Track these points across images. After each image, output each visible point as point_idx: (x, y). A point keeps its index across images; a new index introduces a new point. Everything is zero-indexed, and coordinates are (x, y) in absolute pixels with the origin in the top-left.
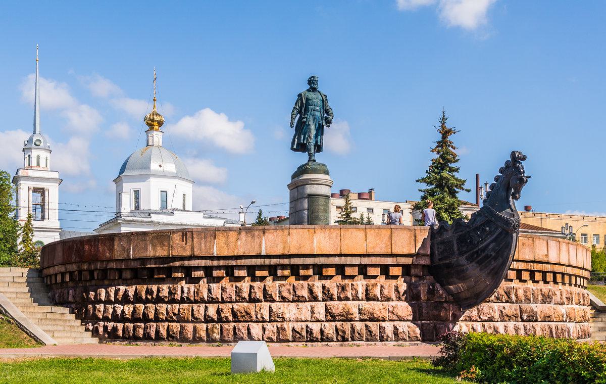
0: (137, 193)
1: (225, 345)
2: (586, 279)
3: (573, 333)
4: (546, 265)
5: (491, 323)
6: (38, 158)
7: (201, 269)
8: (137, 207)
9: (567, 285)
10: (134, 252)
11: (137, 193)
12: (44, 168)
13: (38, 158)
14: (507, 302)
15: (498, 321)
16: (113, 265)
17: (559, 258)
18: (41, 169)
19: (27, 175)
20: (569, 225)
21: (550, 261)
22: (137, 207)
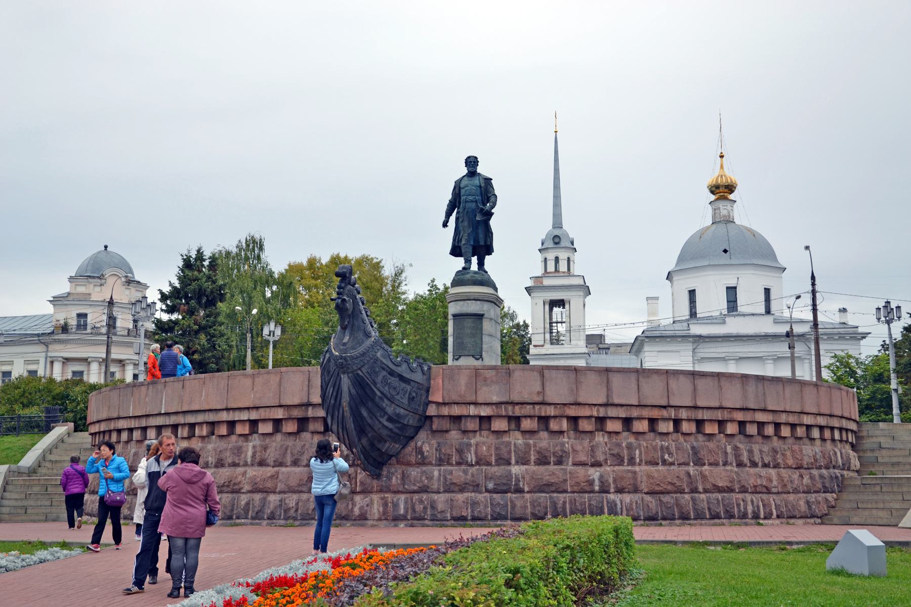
0: (692, 293)
1: (662, 527)
2: (852, 431)
3: (91, 484)
4: (543, 408)
5: (425, 496)
6: (557, 260)
7: (319, 420)
8: (693, 314)
9: (829, 442)
10: (134, 408)
11: (692, 293)
12: (564, 272)
13: (557, 260)
14: (459, 464)
15: (439, 492)
16: (551, 412)
17: (694, 385)
18: (561, 275)
19: (541, 285)
20: (893, 306)
21: (549, 400)
22: (693, 314)
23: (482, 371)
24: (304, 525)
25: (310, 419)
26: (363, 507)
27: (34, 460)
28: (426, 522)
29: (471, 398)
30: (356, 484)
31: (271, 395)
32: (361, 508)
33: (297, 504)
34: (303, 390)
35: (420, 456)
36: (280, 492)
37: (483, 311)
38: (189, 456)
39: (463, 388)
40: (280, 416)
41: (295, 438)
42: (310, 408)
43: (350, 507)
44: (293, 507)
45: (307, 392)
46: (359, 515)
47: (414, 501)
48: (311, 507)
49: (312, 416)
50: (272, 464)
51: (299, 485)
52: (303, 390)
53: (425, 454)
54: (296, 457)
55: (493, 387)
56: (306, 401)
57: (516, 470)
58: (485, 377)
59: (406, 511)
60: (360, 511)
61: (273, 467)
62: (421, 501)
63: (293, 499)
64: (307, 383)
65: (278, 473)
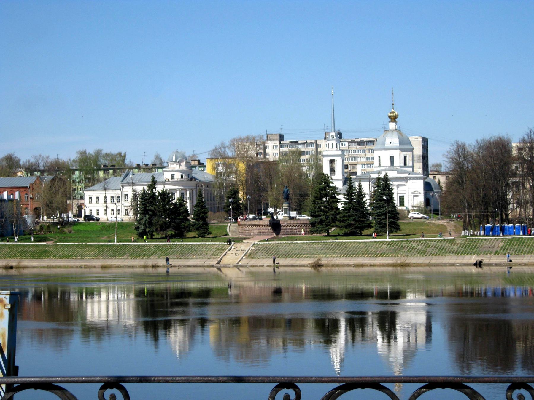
57: (288, 230)
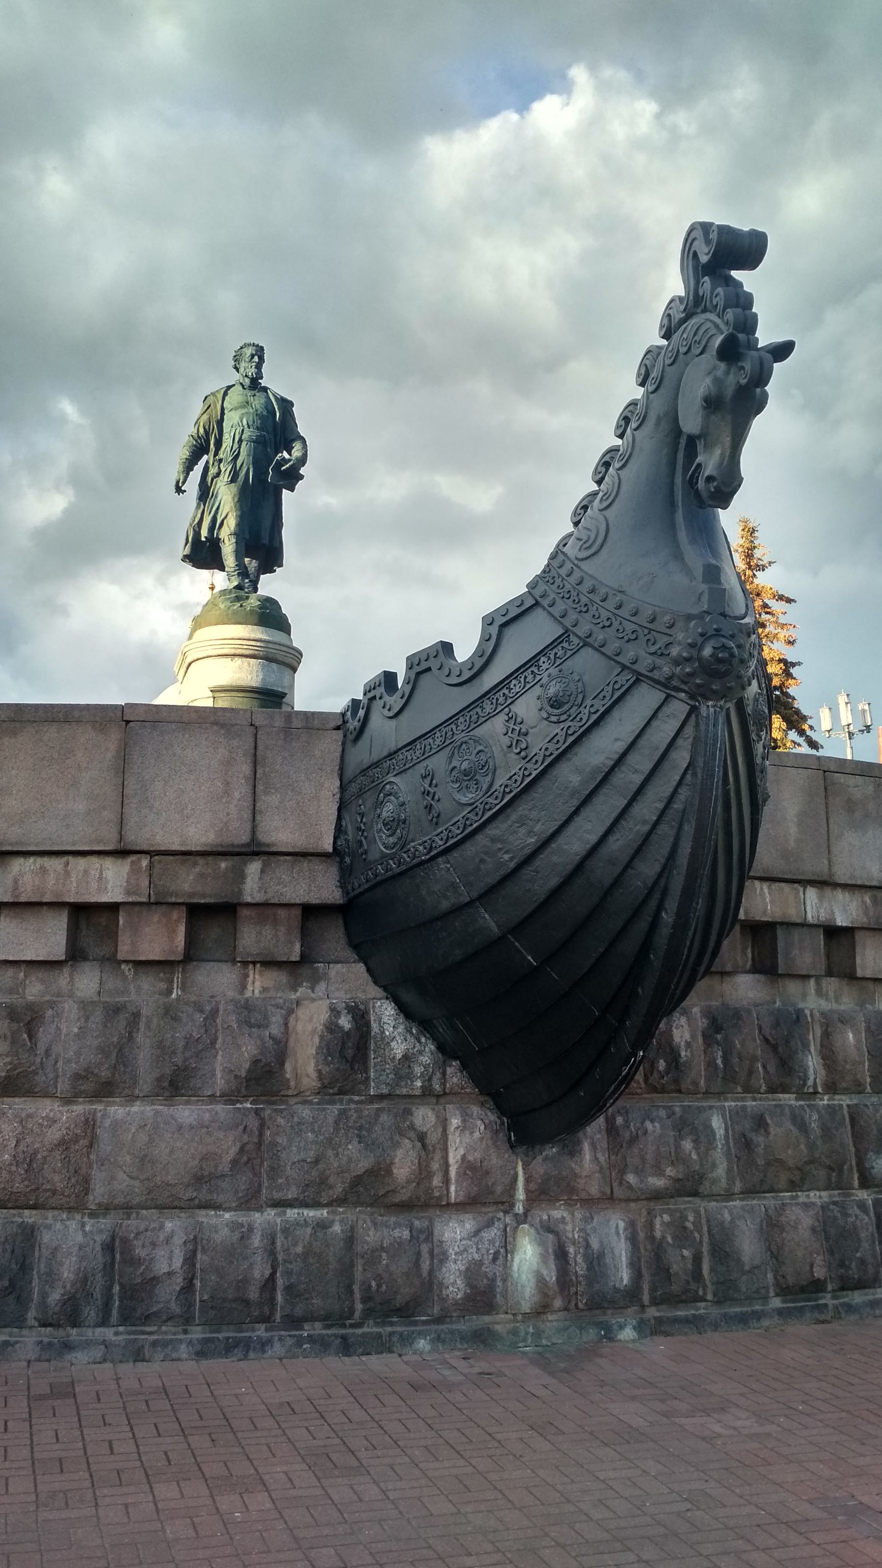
7: (282, 913)
15: (729, 1196)
23: (842, 778)
24: (229, 1348)
25: (245, 912)
26: (480, 1263)
27: (65, 942)
28: (702, 1308)
29: (813, 866)
30: (446, 1172)
31: (81, 806)
32: (471, 1273)
33: (190, 1260)
34: (227, 793)
35: (662, 1065)
36: (105, 1209)
37: (283, 687)
38: (311, 1020)
39: (793, 830)
40: (113, 894)
41: (163, 986)
42: (254, 868)
43: (425, 1265)
44: (170, 1274)
45: (247, 804)
46: (467, 1298)
47: (658, 1234)
48: (257, 1274)
49: (259, 898)
50: (63, 1086)
51: (199, 1180)
52: (227, 793)
53: (683, 1054)
54: (178, 1060)
55: (870, 833)
56: (245, 838)
58: (849, 800)
59: (637, 1276)
60: (469, 1285)
61: (67, 1101)
62: (682, 1235)
63: (168, 1240)
64: (247, 769)
65: (89, 1124)
